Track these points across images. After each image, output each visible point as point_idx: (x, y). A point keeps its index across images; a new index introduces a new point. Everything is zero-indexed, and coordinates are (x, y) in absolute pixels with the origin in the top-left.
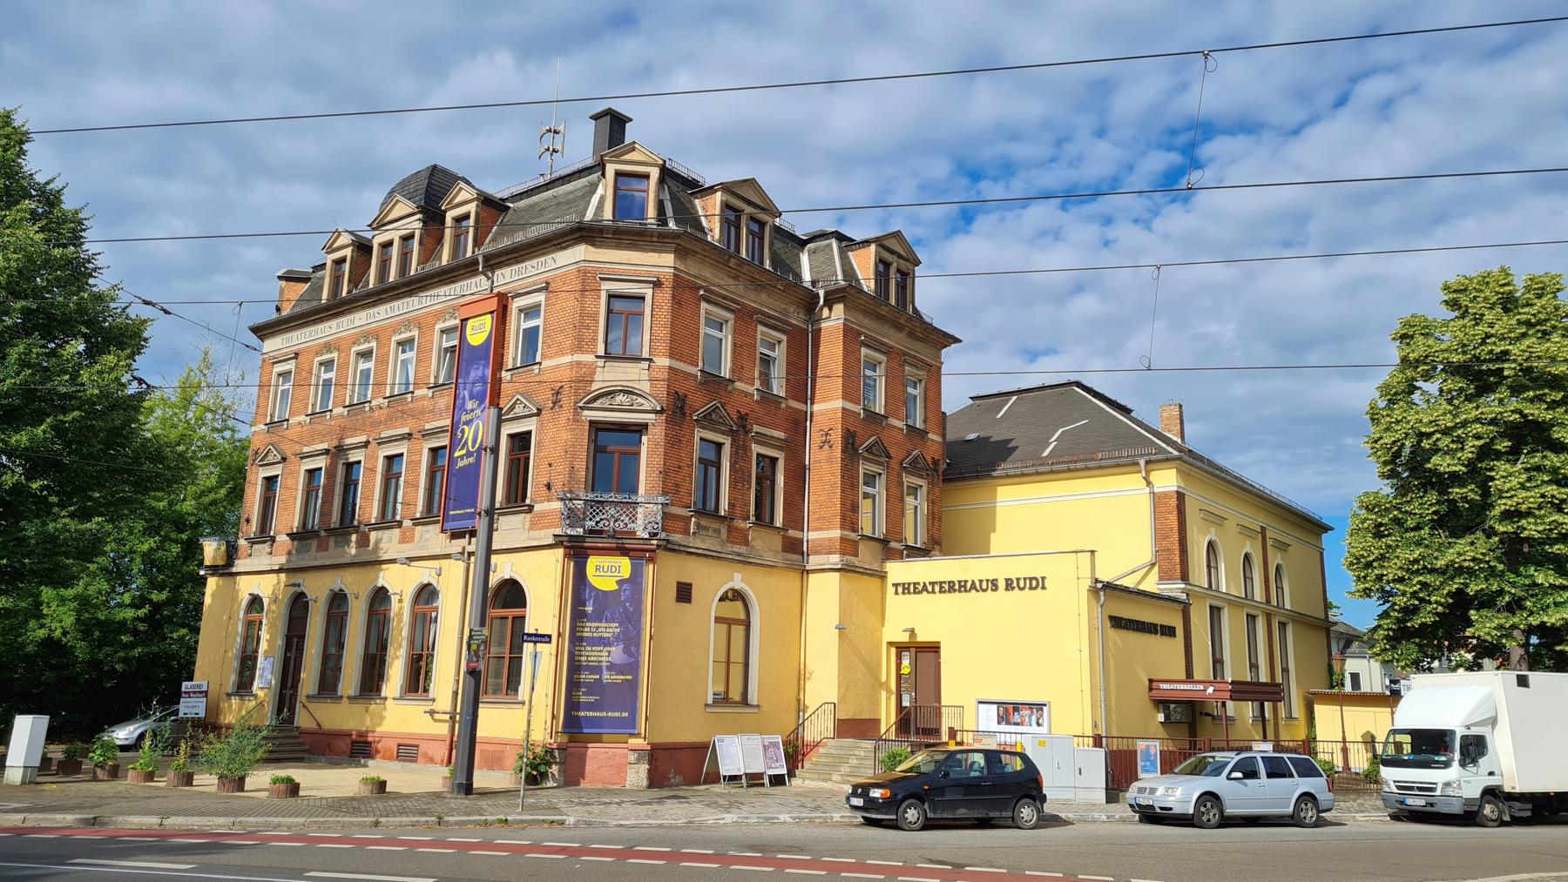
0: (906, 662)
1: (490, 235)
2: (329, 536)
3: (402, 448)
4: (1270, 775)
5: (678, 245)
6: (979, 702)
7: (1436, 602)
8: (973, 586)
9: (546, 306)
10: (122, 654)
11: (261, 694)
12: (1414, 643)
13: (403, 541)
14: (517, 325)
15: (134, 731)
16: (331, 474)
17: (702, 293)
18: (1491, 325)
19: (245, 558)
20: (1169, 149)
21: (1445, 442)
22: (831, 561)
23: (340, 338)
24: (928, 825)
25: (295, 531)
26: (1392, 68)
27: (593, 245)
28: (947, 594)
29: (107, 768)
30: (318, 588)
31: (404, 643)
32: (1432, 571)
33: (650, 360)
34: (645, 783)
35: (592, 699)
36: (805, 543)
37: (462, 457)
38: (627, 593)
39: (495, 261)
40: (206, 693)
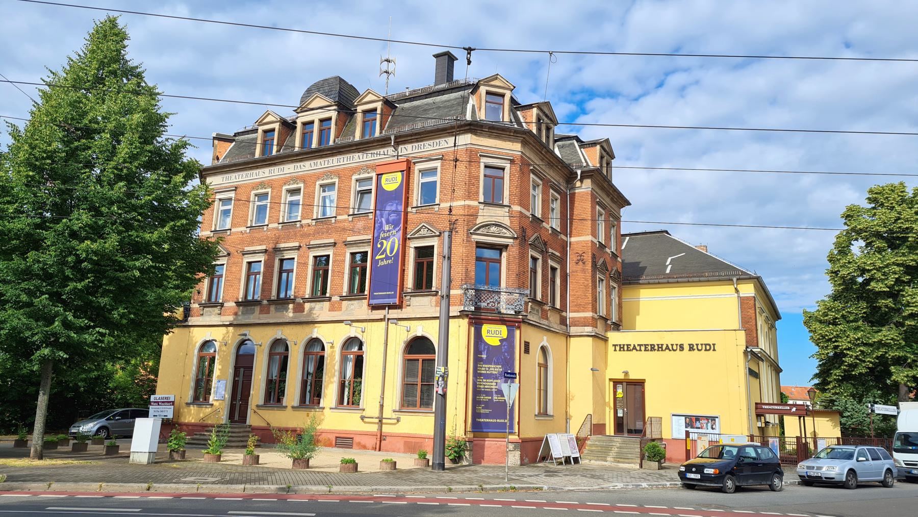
0: (620, 390)
1: (388, 123)
2: (270, 304)
3: (330, 252)
4: (873, 459)
5: (524, 138)
6: (673, 415)
7: (868, 361)
8: (667, 348)
9: (442, 169)
10: (84, 376)
11: (216, 404)
12: (851, 383)
13: (332, 309)
14: (417, 181)
15: (94, 427)
16: (269, 266)
17: (532, 168)
18: (899, 213)
19: (198, 316)
20: (570, 102)
21: (879, 275)
22: (586, 330)
23: (272, 180)
24: (738, 489)
25: (240, 300)
26: (686, 70)
27: (475, 135)
28: (650, 352)
29: (180, 452)
30: (261, 339)
31: (337, 374)
32: (865, 345)
33: (509, 206)
34: (519, 463)
35: (487, 411)
36: (568, 320)
37: (382, 260)
38: (506, 347)
39: (401, 140)
40: (173, 403)
